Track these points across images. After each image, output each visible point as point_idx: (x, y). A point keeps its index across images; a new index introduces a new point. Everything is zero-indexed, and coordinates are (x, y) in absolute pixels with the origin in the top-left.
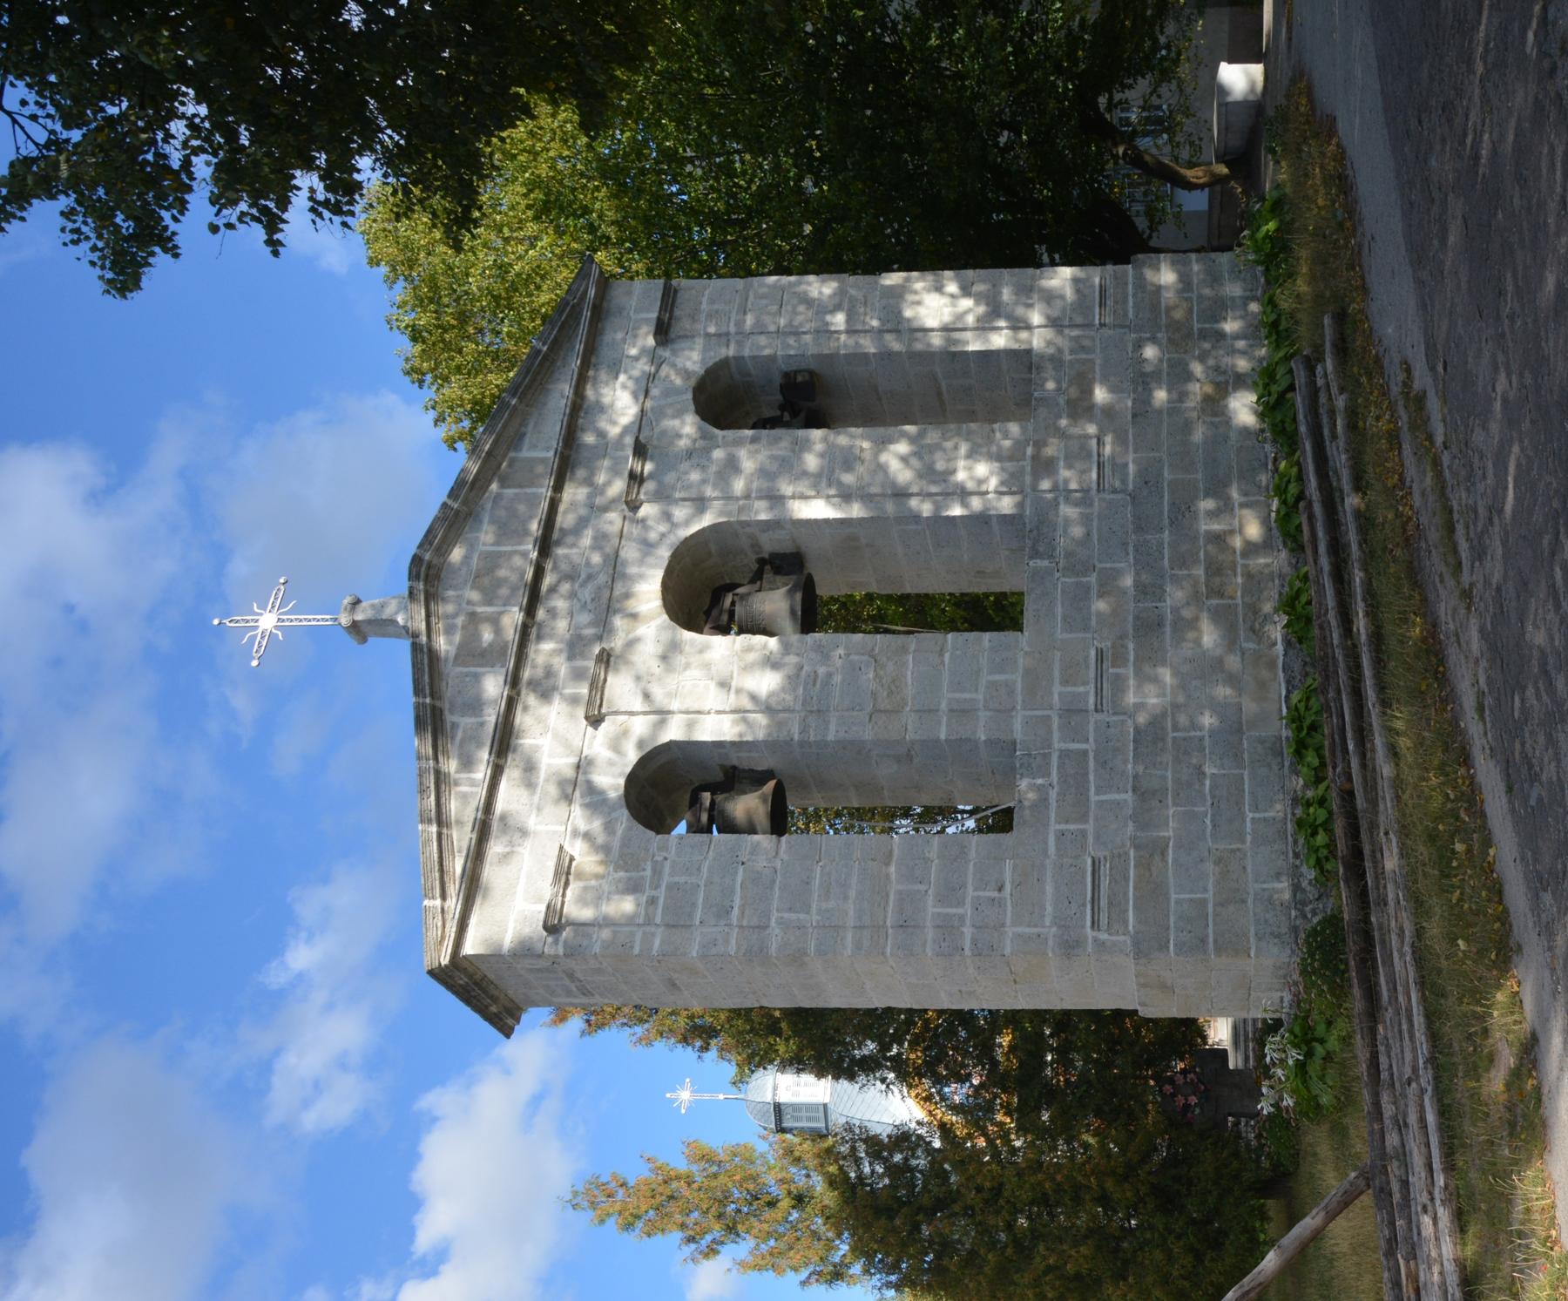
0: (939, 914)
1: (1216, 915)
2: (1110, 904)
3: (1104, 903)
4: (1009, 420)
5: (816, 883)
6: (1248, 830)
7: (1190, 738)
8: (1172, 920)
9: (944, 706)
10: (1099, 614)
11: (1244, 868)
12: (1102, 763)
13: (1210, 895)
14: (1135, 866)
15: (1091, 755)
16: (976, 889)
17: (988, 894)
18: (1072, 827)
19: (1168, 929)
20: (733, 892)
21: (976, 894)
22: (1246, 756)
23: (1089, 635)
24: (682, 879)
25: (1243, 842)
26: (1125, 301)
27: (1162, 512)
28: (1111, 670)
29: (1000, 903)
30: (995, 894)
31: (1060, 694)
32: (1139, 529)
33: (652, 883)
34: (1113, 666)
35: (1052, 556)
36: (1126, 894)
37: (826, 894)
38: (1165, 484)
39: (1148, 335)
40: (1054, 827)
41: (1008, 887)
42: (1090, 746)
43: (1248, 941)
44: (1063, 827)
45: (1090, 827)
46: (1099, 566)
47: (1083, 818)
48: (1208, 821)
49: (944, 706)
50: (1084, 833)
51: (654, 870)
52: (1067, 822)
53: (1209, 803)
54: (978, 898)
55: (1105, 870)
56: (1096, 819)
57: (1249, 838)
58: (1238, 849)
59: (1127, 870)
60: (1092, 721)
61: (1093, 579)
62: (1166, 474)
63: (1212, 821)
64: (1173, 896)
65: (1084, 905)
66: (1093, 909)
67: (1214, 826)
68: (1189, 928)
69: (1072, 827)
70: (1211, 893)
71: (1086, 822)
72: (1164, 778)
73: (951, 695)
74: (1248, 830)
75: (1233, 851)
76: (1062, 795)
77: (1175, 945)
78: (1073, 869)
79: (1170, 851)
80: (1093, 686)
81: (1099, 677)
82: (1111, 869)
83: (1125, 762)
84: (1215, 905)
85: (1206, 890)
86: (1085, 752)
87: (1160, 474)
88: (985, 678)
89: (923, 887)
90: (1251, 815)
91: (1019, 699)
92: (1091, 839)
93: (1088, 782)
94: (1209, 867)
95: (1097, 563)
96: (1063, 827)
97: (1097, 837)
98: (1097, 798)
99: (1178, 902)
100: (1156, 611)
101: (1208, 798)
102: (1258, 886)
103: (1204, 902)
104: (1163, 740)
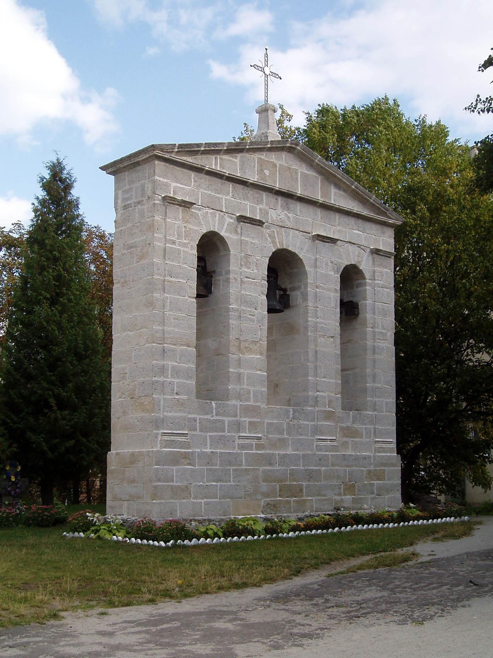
8: (166, 467)
12: (221, 438)
13: (175, 484)
15: (223, 434)
17: (175, 388)
18: (198, 425)
20: (177, 278)
25: (193, 499)
27: (309, 466)
29: (172, 394)
30: (175, 392)
31: (245, 421)
40: (198, 417)
41: (177, 397)
44: (198, 421)
45: (198, 433)
47: (201, 430)
50: (195, 430)
53: (207, 484)
54: (174, 384)
56: (200, 435)
64: (175, 468)
67: (199, 486)
69: (198, 425)
85: (177, 482)
86: (224, 431)
92: (193, 433)
96: (198, 421)
104: (230, 465)
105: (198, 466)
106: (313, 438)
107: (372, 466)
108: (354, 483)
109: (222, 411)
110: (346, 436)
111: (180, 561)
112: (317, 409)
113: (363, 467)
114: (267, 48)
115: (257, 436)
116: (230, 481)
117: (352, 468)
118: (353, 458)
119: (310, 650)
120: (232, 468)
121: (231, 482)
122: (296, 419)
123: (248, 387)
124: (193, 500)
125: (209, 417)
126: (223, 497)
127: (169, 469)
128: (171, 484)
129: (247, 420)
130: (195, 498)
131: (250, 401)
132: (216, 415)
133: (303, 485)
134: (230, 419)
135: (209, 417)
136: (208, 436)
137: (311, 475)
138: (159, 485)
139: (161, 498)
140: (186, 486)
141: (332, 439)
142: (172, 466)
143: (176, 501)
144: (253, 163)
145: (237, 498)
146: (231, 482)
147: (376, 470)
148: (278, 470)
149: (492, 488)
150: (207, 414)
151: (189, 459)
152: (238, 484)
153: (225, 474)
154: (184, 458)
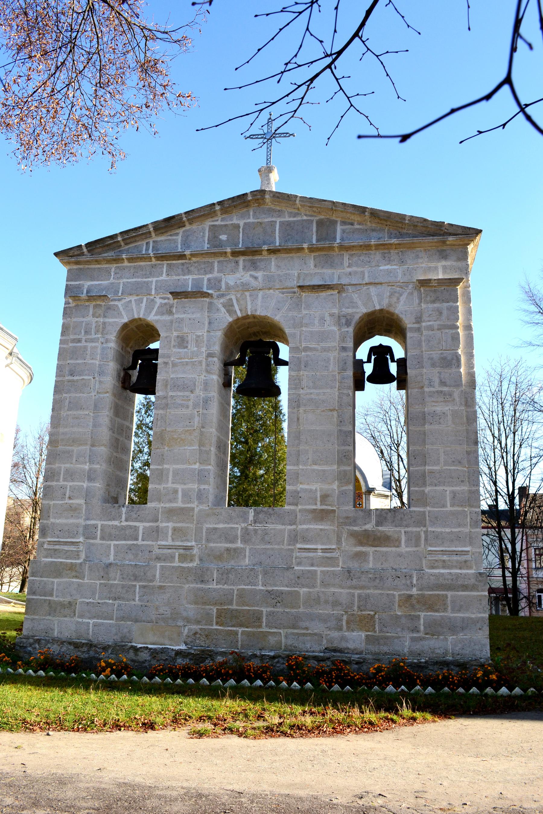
0: (60, 470)
1: (45, 600)
2: (55, 550)
3: (57, 547)
6: (84, 620)
7: (135, 594)
8: (45, 579)
9: (166, 466)
11: (66, 616)
12: (130, 548)
13: (54, 598)
14: (72, 563)
15: (135, 542)
16: (70, 486)
17: (68, 492)
18: (99, 532)
19: (41, 577)
20: (80, 375)
21: (68, 487)
22: (122, 622)
23: (204, 542)
24: (89, 352)
25: (78, 617)
26: (444, 567)
27: (276, 586)
29: (63, 498)
30: (67, 496)
31: (167, 526)
33: (88, 339)
34: (179, 555)
35: (255, 522)
36: (59, 557)
39: (415, 582)
42: (140, 542)
43: (31, 615)
45: (98, 541)
48: (91, 600)
49: (166, 466)
52: (101, 530)
53: (99, 601)
54: (66, 488)
55: (72, 548)
56: (101, 544)
57: (81, 620)
58: (75, 615)
59: (71, 559)
60: (154, 543)
62: (305, 589)
64: (56, 580)
66: (55, 542)
67: (88, 603)
68: (40, 587)
69: (99, 532)
70: (56, 599)
71: (101, 539)
72: (115, 580)
73: (171, 470)
74: (84, 620)
75: (74, 612)
77: (33, 580)
78: (75, 532)
79: (78, 580)
80: (171, 544)
81: (177, 548)
82: (72, 551)
84: (49, 600)
85: (57, 597)
86: (137, 539)
88: (180, 487)
91: (167, 505)
98: (112, 545)
99: (53, 582)
100: (211, 580)
101: (103, 601)
103: (51, 595)
104: (135, 580)
105: (88, 579)
106: (293, 547)
107: (415, 589)
108: (372, 613)
109: (135, 516)
110: (361, 544)
111: (272, 647)
112: (300, 507)
113: (394, 589)
115: (185, 545)
116: (134, 600)
117: (368, 591)
118: (370, 576)
120: (138, 584)
121: (135, 601)
122: (260, 523)
123: (174, 486)
124: (77, 619)
125: (116, 523)
126: (123, 619)
127: (48, 581)
128: (50, 598)
129: (171, 525)
130: (81, 616)
131: (177, 502)
132: (126, 520)
133: (262, 611)
134: (147, 525)
135: (116, 523)
136: (112, 545)
137: (278, 599)
138: (33, 599)
140: (70, 602)
141: (326, 549)
142: (53, 578)
143: (54, 619)
144: (202, 234)
145: (144, 621)
146: (135, 601)
147: (423, 596)
148: (215, 590)
149: (56, 260)
151: (76, 571)
152: (147, 604)
153: (127, 591)
154: (69, 570)
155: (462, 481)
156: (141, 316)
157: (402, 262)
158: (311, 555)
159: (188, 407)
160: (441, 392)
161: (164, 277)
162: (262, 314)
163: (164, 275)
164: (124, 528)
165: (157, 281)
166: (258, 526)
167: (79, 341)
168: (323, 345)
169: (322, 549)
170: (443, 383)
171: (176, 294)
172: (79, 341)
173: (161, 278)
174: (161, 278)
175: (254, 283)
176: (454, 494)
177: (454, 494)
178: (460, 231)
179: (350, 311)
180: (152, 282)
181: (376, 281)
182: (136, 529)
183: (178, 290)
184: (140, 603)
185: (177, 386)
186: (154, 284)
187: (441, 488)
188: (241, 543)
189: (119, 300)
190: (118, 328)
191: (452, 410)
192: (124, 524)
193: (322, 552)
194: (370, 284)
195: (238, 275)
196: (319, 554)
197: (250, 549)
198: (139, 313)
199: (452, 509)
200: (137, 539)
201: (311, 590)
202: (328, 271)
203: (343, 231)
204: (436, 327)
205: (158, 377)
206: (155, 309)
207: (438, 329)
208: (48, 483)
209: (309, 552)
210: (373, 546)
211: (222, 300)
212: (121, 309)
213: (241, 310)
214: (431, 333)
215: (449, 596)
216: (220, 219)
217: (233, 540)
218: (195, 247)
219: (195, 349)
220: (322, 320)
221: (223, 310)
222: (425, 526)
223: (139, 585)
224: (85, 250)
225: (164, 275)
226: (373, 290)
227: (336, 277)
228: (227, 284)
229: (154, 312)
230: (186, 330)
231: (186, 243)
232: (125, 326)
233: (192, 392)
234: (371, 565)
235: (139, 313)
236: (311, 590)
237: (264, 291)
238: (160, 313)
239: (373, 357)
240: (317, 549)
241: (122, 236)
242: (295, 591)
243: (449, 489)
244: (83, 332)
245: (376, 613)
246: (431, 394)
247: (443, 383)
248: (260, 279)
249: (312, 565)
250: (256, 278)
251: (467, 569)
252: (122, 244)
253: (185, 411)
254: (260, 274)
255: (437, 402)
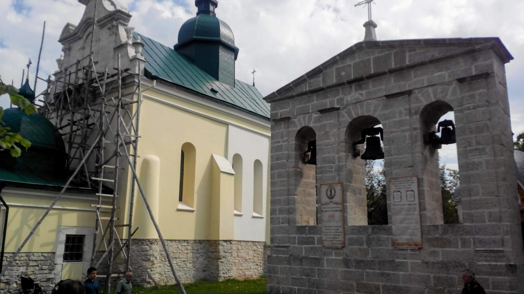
3: (279, 249)
4: (352, 121)
5: (283, 179)
10: (33, 289)
12: (312, 248)
17: (281, 220)
28: (334, 252)
29: (279, 223)
30: (281, 222)
32: (380, 263)
34: (335, 253)
37: (281, 182)
38: (397, 272)
40: (296, 236)
41: (282, 225)
44: (297, 238)
45: (296, 245)
46: (370, 249)
47: (299, 244)
48: (295, 277)
50: (295, 244)
51: (286, 140)
55: (285, 249)
61: (365, 246)
62: (402, 273)
63: (295, 278)
65: (279, 244)
69: (297, 241)
75: (289, 282)
76: (304, 238)
83: (312, 255)
85: (280, 274)
86: (314, 244)
87: (401, 271)
89: (282, 204)
90: (297, 288)
92: (294, 245)
93: (307, 245)
94: (285, 276)
95: (371, 248)
96: (297, 238)
97: (294, 247)
102: (281, 288)
114: (256, 69)
118: (440, 265)
119: (240, 254)
125: (304, 236)
135: (304, 236)
139: (381, 245)
150: (302, 233)
155: (495, 206)
156: (306, 125)
157: (447, 69)
158: (404, 252)
159: (332, 172)
160: (478, 149)
161: (315, 102)
162: (367, 115)
163: (315, 101)
164: (308, 238)
165: (312, 105)
166: (374, 236)
167: (279, 142)
168: (401, 128)
169: (410, 249)
170: (478, 143)
171: (322, 111)
172: (279, 142)
173: (313, 103)
174: (313, 103)
175: (361, 98)
176: (490, 214)
177: (490, 214)
178: (436, 53)
179: (417, 105)
180: (309, 106)
181: (432, 84)
182: (313, 238)
183: (322, 108)
184: (318, 279)
185: (325, 161)
186: (310, 106)
187: (481, 210)
188: (366, 245)
189: (295, 118)
190: (296, 133)
191: (485, 160)
192: (308, 236)
193: (410, 251)
194: (428, 86)
195: (352, 95)
196: (409, 252)
197: (371, 249)
198: (305, 123)
199: (489, 223)
200: (314, 244)
201: (405, 273)
202: (402, 83)
203: (410, 56)
204: (472, 108)
205: (317, 157)
206: (312, 121)
207: (473, 109)
208: (273, 216)
209: (403, 251)
210: (441, 248)
211: (345, 110)
212: (296, 122)
213: (355, 114)
214: (468, 111)
215: (490, 279)
216: (340, 63)
217: (361, 245)
218: (329, 83)
219: (408, 117)
220: (400, 113)
221: (346, 115)
222: (473, 235)
223: (317, 269)
224: (276, 94)
225: (315, 101)
226: (430, 90)
227: (407, 85)
228: (347, 101)
229: (312, 123)
230: (328, 130)
231: (324, 81)
232: (300, 131)
233: (334, 163)
234: (441, 259)
235: (305, 123)
236: (405, 273)
237: (367, 101)
238: (315, 122)
239: (441, 128)
240: (407, 249)
241: (292, 84)
242: (397, 273)
243: (486, 211)
244: (280, 137)
245: (445, 288)
246: (471, 151)
247: (478, 143)
248: (364, 94)
249: (405, 259)
250: (362, 94)
251: (501, 262)
252: (294, 87)
253: (331, 174)
254: (364, 92)
255: (475, 156)
